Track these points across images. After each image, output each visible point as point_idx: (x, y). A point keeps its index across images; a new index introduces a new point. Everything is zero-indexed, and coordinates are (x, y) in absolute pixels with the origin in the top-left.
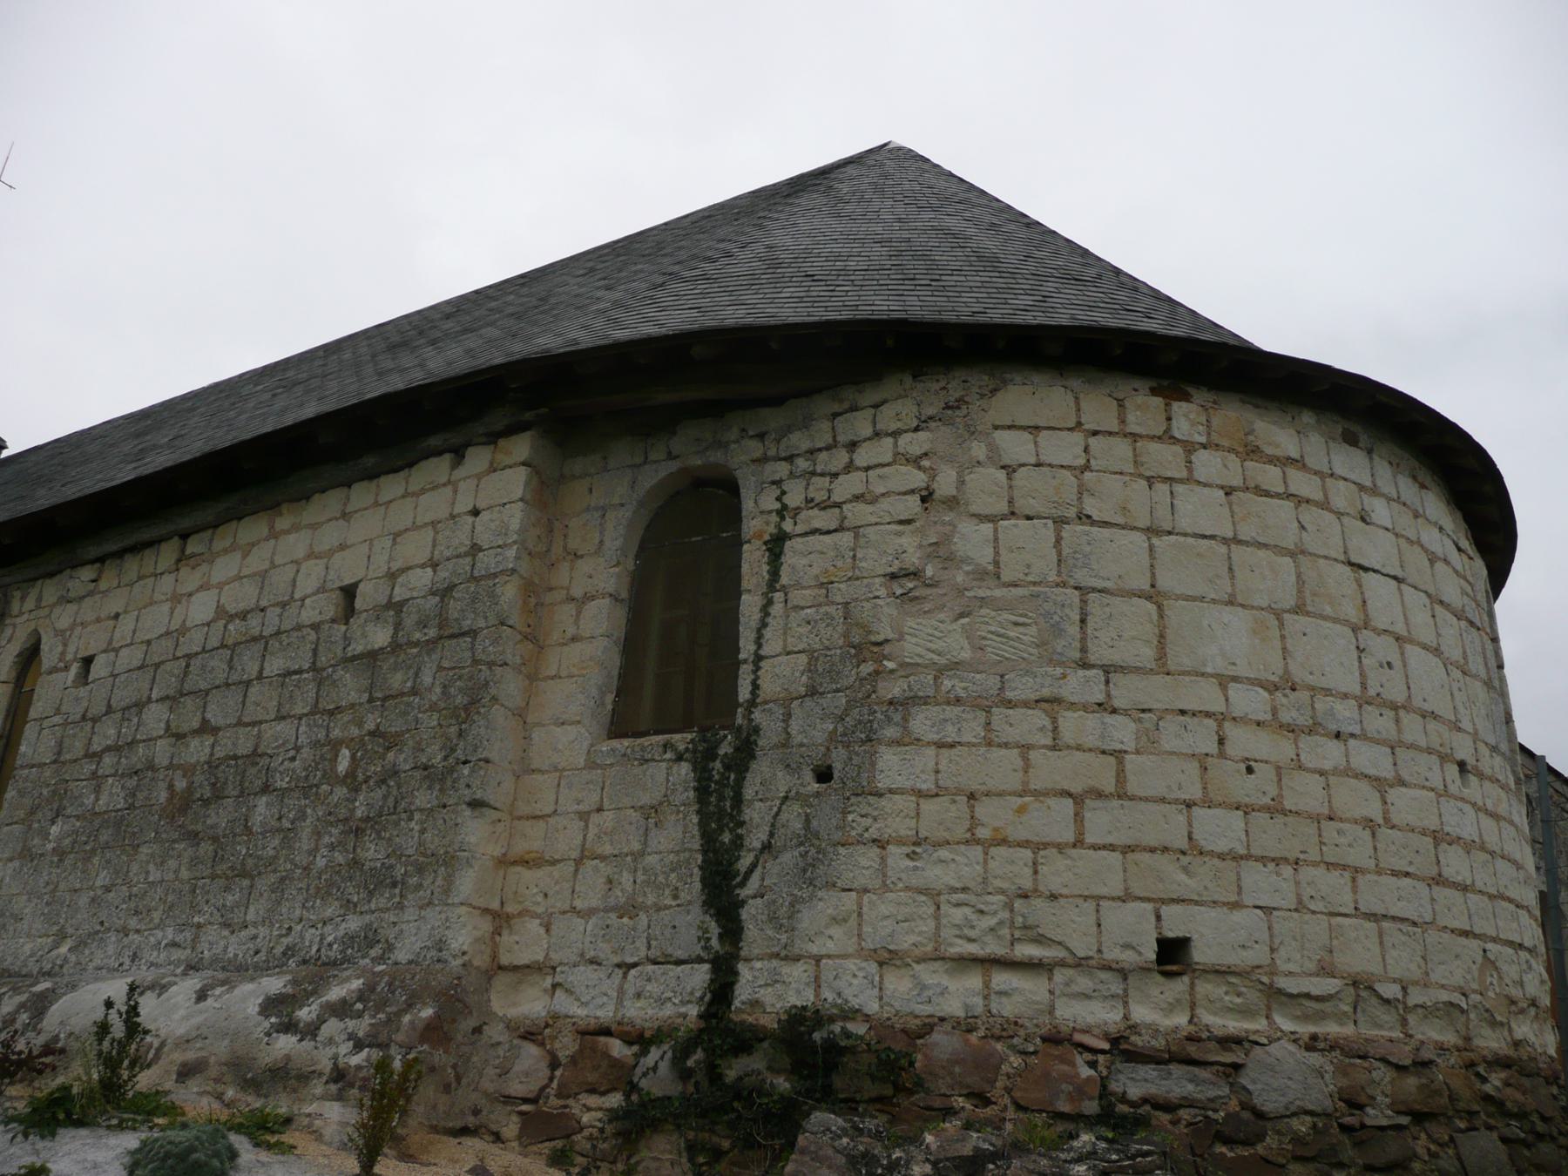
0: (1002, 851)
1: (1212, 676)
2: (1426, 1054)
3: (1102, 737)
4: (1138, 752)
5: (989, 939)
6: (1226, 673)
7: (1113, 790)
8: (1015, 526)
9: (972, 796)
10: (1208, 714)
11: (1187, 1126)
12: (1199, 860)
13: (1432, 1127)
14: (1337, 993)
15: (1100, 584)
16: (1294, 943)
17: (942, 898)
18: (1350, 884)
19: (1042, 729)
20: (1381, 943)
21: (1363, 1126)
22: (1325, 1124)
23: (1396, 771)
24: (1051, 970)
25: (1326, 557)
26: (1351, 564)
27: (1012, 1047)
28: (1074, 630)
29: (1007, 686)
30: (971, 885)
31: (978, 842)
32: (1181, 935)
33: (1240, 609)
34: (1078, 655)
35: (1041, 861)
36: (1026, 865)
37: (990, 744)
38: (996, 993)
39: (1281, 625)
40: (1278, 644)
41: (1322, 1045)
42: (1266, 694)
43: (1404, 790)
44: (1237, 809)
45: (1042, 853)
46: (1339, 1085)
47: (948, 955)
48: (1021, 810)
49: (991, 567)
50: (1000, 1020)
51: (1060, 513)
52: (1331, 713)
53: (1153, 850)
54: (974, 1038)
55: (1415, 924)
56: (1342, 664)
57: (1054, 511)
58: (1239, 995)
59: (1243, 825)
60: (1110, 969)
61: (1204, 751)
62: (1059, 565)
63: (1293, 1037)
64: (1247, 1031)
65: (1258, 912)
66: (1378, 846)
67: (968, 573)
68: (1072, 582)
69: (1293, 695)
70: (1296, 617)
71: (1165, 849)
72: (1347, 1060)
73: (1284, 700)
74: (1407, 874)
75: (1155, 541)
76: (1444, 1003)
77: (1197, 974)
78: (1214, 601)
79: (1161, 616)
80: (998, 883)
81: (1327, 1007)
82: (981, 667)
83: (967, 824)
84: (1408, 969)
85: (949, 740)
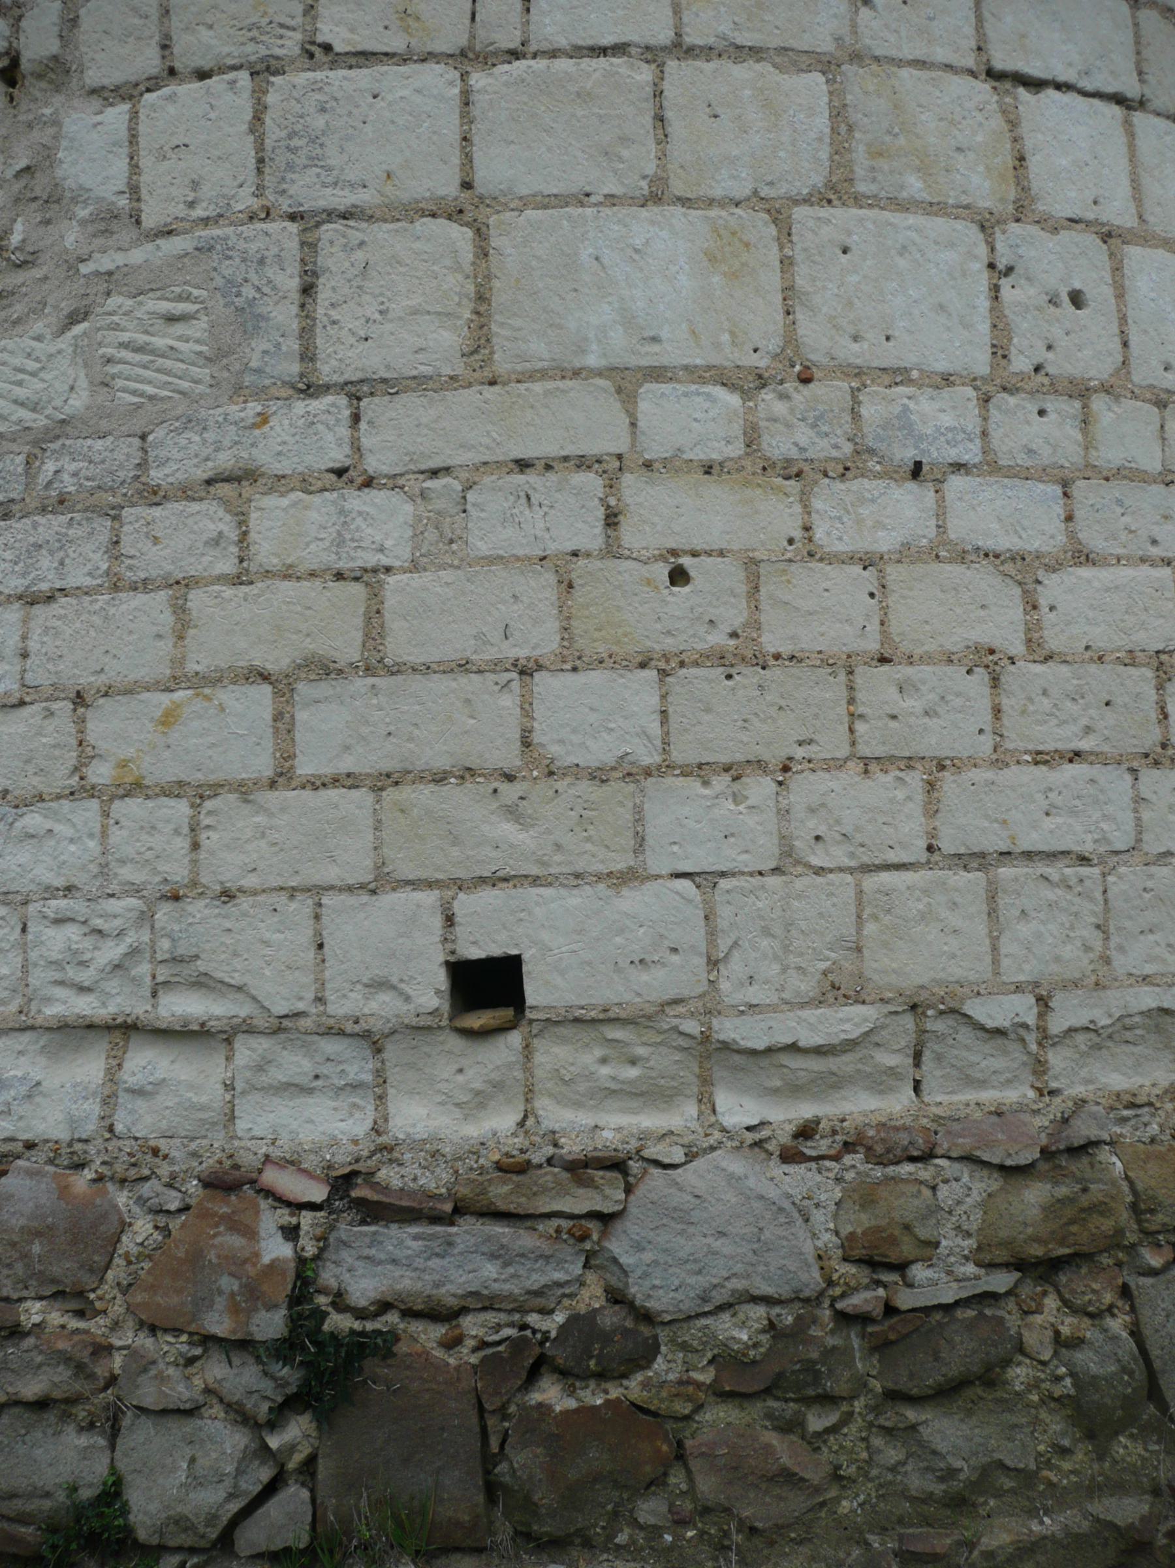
0: (131, 809)
1: (600, 373)
2: (1083, 1130)
3: (340, 542)
4: (415, 567)
5: (112, 985)
6: (633, 361)
7: (356, 656)
8: (171, 98)
9: (79, 699)
10: (582, 463)
11: (475, 1350)
12: (544, 788)
13: (1073, 1281)
14: (867, 1034)
15: (342, 199)
16: (765, 943)
17: (32, 908)
18: (920, 797)
19: (216, 541)
20: (992, 913)
21: (890, 1310)
22: (799, 1318)
23: (1072, 535)
24: (229, 1041)
25: (919, 64)
26: (993, 75)
27: (141, 1201)
28: (285, 314)
29: (152, 454)
30: (80, 879)
31: (92, 792)
32: (496, 951)
33: (679, 210)
34: (295, 368)
35: (207, 821)
36: (177, 832)
37: (115, 588)
38: (132, 1091)
39: (786, 233)
40: (772, 280)
41: (822, 1145)
42: (733, 400)
43: (1085, 572)
44: (643, 665)
45: (209, 805)
46: (846, 1230)
47: (39, 1021)
48: (168, 719)
49: (123, 202)
50: (128, 1146)
51: (263, 51)
52: (903, 423)
53: (440, 778)
54: (81, 1181)
55: (1084, 860)
56: (942, 307)
57: (250, 48)
58: (633, 1062)
59: (655, 700)
60: (342, 1033)
61: (570, 546)
62: (259, 171)
63: (750, 1137)
64: (643, 1137)
65: (685, 885)
66: (1006, 703)
67: (83, 223)
68: (285, 206)
69: (802, 395)
70: (824, 212)
71: (468, 773)
72: (878, 1172)
73: (780, 408)
74: (1076, 756)
75: (478, 80)
76: (1146, 1014)
77: (536, 1028)
78: (611, 200)
79: (483, 253)
80: (127, 873)
81: (843, 1064)
82: (104, 425)
83: (71, 757)
84: (1057, 959)
85: (44, 586)
